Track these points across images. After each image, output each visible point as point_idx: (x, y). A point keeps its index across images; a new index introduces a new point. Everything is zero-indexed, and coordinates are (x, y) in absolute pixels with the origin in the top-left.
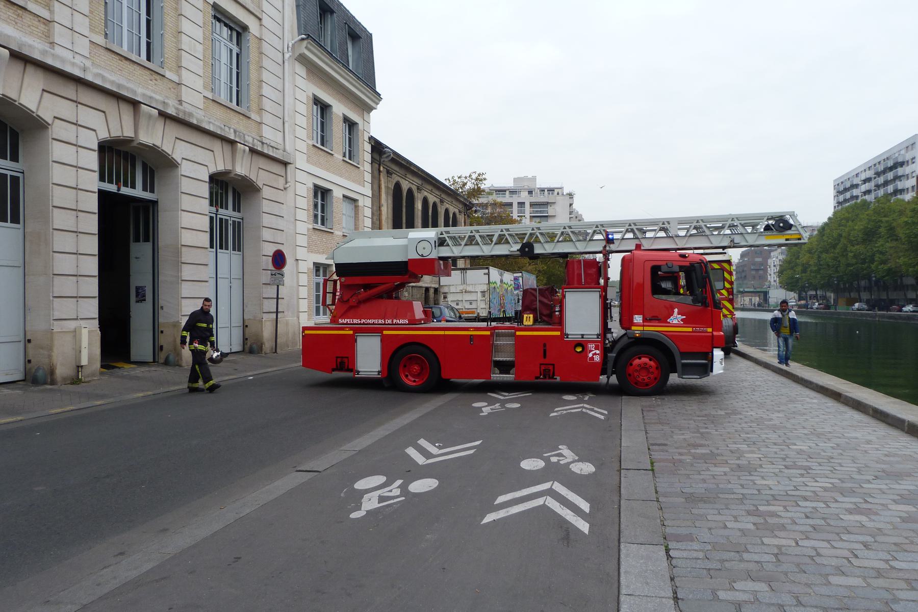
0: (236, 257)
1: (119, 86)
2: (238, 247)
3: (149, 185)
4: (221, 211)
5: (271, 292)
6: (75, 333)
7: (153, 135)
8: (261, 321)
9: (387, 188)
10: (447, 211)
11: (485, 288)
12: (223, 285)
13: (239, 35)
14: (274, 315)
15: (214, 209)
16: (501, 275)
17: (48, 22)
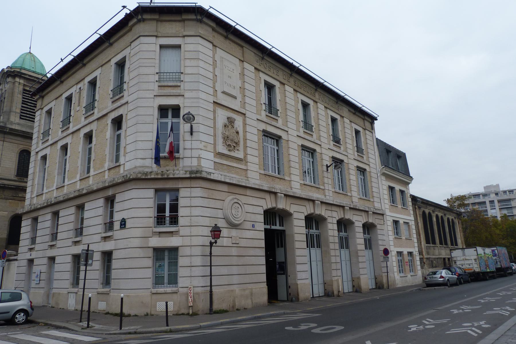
0: (318, 251)
1: (340, 203)
2: (319, 246)
3: (282, 224)
4: (340, 233)
5: (384, 264)
6: (337, 280)
7: (282, 204)
9: (419, 214)
10: (448, 219)
11: (476, 257)
12: (344, 263)
13: (312, 154)
14: (386, 274)
15: (307, 230)
16: (484, 250)
17: (324, 190)
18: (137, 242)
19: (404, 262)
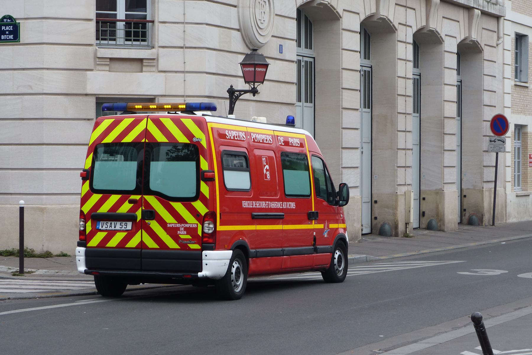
8: (481, 191)
18: (56, 82)
19: (525, 156)
